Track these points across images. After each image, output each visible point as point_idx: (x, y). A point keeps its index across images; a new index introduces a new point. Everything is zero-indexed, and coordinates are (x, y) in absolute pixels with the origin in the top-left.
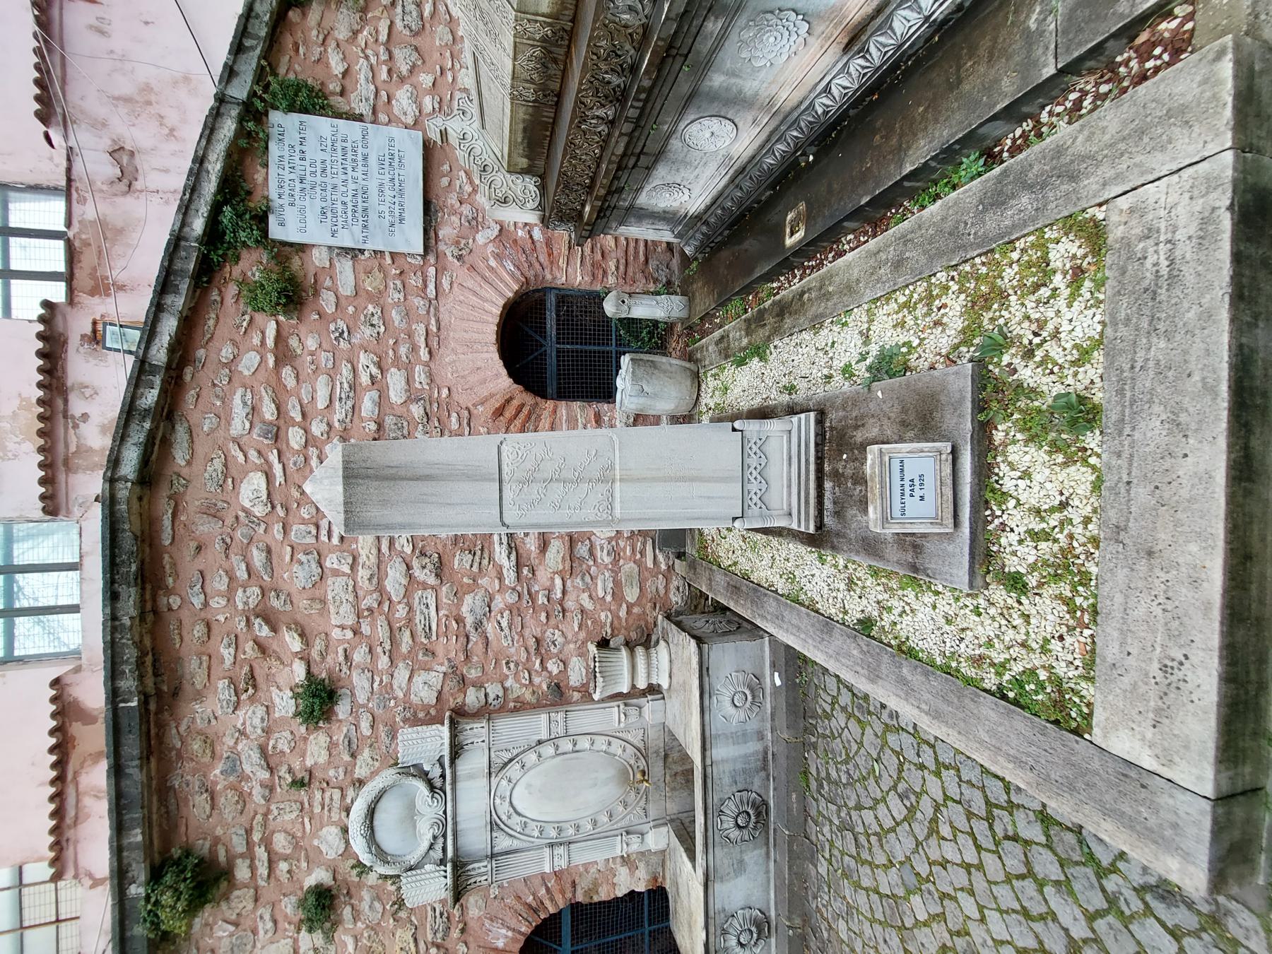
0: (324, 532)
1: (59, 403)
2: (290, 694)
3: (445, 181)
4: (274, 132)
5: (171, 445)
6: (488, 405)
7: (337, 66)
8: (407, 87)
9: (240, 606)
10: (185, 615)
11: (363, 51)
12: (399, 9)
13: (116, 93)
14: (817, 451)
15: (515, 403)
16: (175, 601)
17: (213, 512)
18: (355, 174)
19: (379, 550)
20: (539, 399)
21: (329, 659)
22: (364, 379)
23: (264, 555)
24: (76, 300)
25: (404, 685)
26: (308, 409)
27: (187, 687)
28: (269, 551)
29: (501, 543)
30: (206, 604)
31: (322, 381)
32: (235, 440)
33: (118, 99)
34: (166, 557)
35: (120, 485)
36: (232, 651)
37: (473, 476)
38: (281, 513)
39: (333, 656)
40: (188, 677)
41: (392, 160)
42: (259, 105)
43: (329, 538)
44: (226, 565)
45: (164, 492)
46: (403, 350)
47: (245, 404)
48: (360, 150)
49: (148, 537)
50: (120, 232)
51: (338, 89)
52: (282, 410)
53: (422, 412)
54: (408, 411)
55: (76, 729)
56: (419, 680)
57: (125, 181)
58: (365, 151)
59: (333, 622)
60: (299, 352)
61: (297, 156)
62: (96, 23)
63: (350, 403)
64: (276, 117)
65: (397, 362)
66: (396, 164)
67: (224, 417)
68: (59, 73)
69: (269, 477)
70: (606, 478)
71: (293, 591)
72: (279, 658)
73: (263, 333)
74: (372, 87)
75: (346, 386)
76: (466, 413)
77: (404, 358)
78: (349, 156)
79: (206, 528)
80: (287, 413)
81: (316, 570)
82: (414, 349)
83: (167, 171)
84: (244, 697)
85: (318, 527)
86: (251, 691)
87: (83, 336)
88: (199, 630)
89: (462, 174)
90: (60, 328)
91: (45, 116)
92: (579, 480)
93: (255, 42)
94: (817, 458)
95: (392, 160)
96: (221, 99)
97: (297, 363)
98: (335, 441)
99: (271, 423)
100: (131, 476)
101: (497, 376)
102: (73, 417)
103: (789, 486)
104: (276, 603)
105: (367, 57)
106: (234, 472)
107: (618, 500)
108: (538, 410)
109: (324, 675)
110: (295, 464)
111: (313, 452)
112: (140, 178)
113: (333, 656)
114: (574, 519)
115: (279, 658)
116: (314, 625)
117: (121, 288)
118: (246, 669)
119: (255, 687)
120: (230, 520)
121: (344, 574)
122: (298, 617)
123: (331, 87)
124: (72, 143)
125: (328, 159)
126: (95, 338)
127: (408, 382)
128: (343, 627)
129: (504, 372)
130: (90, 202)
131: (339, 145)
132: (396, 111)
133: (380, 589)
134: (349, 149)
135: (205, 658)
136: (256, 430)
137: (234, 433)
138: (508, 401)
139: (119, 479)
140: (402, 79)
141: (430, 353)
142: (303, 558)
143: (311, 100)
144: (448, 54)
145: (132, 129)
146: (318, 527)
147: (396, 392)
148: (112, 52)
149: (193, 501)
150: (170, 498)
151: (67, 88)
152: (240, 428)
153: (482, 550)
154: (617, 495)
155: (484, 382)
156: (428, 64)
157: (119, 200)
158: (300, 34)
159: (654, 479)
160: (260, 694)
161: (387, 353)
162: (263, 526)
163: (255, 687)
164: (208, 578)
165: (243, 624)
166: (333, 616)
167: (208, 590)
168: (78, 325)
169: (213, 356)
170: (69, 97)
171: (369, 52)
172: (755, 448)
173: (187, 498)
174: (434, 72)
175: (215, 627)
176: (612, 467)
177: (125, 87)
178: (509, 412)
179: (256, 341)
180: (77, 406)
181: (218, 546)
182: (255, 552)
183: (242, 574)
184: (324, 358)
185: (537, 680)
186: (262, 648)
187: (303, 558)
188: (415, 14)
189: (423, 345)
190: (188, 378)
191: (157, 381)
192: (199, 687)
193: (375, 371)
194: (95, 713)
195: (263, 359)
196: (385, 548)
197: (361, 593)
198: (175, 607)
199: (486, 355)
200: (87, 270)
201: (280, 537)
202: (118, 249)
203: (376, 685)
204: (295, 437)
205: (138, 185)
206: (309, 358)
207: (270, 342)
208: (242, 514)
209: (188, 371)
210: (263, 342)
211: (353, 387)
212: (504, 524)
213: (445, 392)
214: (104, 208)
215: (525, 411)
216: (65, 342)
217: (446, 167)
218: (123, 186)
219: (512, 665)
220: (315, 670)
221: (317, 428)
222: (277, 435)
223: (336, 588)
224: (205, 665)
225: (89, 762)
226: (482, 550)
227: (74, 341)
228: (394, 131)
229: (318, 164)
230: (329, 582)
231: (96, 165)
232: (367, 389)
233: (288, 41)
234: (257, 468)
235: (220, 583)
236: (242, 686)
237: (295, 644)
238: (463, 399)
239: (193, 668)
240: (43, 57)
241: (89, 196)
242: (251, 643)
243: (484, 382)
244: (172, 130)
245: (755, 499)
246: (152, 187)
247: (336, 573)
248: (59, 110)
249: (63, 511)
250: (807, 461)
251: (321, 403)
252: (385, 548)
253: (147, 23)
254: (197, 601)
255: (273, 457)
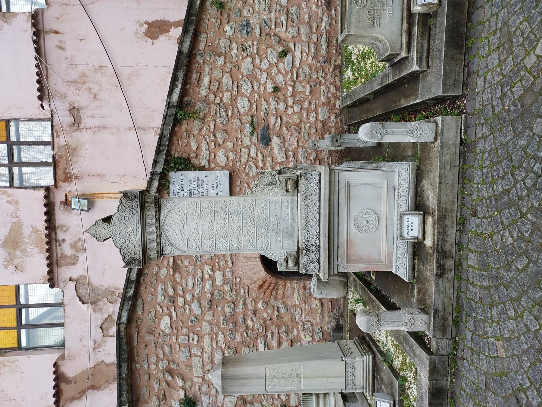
0: (191, 339)
1: (53, 234)
2: (179, 403)
3: (238, 189)
4: (171, 180)
5: (136, 307)
6: (256, 284)
7: (194, 146)
8: (222, 150)
9: (161, 368)
10: (141, 371)
11: (204, 137)
12: (218, 116)
13: (70, 79)
14: (373, 369)
15: (268, 282)
16: (138, 366)
17: (151, 332)
18: (203, 194)
19: (212, 346)
20: (278, 279)
21: (193, 389)
22: (207, 276)
23: (169, 348)
24: (58, 185)
25: (221, 401)
26: (185, 289)
27: (141, 398)
28: (171, 347)
29: (261, 344)
30: (149, 367)
31: (190, 277)
32: (159, 304)
33: (71, 82)
34: (135, 349)
35: (121, 326)
36: (158, 385)
37: (258, 378)
38: (176, 332)
39: (194, 388)
40: (142, 394)
41: (217, 185)
42: (165, 171)
43: (193, 341)
44: (156, 352)
45: (134, 325)
46: (222, 263)
47: (162, 289)
48: (204, 183)
49: (129, 343)
50: (75, 150)
51: (195, 156)
52: (176, 290)
53: (229, 288)
54: (224, 288)
55: (63, 386)
56: (227, 400)
57: (76, 124)
58: (207, 183)
59: (195, 375)
60: (181, 266)
61: (180, 189)
62: (58, 44)
63: (201, 286)
64: (172, 174)
65: (219, 269)
66: (218, 187)
67: (155, 295)
68: (46, 74)
69: (171, 317)
70: (299, 377)
71: (180, 362)
72: (174, 388)
73: (168, 260)
74: (208, 152)
75: (199, 279)
76: (247, 288)
77: (222, 266)
78: (200, 187)
79: (148, 338)
80: (177, 291)
81: (188, 354)
82: (226, 262)
83: (94, 117)
84: (162, 403)
85: (189, 337)
86: (164, 401)
87: (61, 202)
88: (146, 377)
89: (245, 185)
90: (52, 200)
91: (40, 98)
92: (290, 378)
93: (164, 148)
94: (373, 371)
95: (217, 185)
96: (153, 173)
97: (181, 270)
98: (195, 302)
99: (171, 296)
100: (125, 322)
101: (260, 271)
102: (59, 241)
103: (363, 378)
104: (173, 367)
105: (206, 140)
106: (158, 316)
107: (302, 384)
108: (277, 285)
109: (191, 396)
110: (180, 312)
111: (187, 307)
112: (82, 122)
113: (194, 388)
114: (288, 390)
115: (174, 388)
116: (187, 375)
117: (77, 178)
118: (163, 392)
119: (166, 399)
120: (157, 335)
121: (199, 356)
122: (181, 372)
123: (192, 156)
124: (53, 107)
125: (192, 189)
126: (67, 203)
127: (223, 276)
128: (198, 377)
129: (263, 269)
130: (62, 137)
131: (196, 182)
132: (218, 161)
133: (213, 362)
134: (200, 183)
135: (148, 388)
136: (166, 300)
137: (158, 301)
138: (264, 282)
139: (121, 323)
140: (220, 146)
141: (232, 263)
142: (184, 349)
143: (186, 164)
144: (239, 132)
145: (78, 97)
146: (189, 337)
147: (219, 280)
148: (67, 58)
149: (144, 328)
150: (136, 327)
151: (49, 80)
152: (160, 299)
153: (253, 346)
154: (302, 382)
155: (254, 274)
156: (230, 137)
157: (74, 134)
158: (179, 135)
159: (314, 377)
160: (168, 402)
161: (215, 264)
162: (169, 337)
163: (166, 399)
164: (149, 357)
165: (162, 375)
166: (194, 373)
167: (150, 362)
168: (59, 197)
169: (150, 271)
170: (50, 84)
171: (206, 137)
172: (350, 366)
173: (142, 326)
174: (233, 141)
175: (152, 376)
176: (300, 374)
177: (73, 75)
178: (265, 287)
179: (166, 264)
180: (60, 236)
181: (153, 345)
182: (166, 346)
183: (161, 356)
184: (191, 269)
185: (276, 402)
186: (168, 384)
187: (184, 349)
188: (225, 116)
189: (230, 261)
190: (142, 281)
191: (133, 286)
192: (146, 399)
193: (210, 272)
194: (71, 379)
195: (168, 271)
196: (214, 346)
197: (205, 364)
198: (138, 368)
199: (255, 263)
200: (62, 170)
201: (175, 341)
202: (75, 159)
203: (210, 401)
204: (180, 301)
205: (82, 126)
206: (185, 269)
207: (171, 264)
208: (161, 332)
209: (142, 278)
210: (168, 264)
211: (202, 279)
212: (266, 391)
213: (238, 279)
214: (68, 139)
215: (272, 285)
216: (54, 206)
217: (239, 183)
218: (75, 127)
219: (265, 396)
220: (188, 394)
221: (189, 297)
222: (173, 300)
223: (195, 361)
224: (148, 390)
225: (68, 402)
226: (253, 346)
227: (58, 205)
228: (218, 173)
229: (188, 191)
230: (193, 359)
231: (64, 118)
232: (208, 280)
233: (175, 139)
234: (167, 314)
235: (154, 359)
236: (161, 399)
237: (181, 383)
238: (246, 282)
239: (144, 390)
240: (39, 69)
241: (61, 133)
242: (165, 382)
243: (254, 274)
244: (95, 95)
245: (350, 382)
246: (88, 126)
247: (196, 355)
248: (46, 92)
249: (56, 285)
250: (369, 371)
251: (190, 287)
252: (214, 346)
253: (81, 40)
254: (146, 366)
255: (172, 310)
